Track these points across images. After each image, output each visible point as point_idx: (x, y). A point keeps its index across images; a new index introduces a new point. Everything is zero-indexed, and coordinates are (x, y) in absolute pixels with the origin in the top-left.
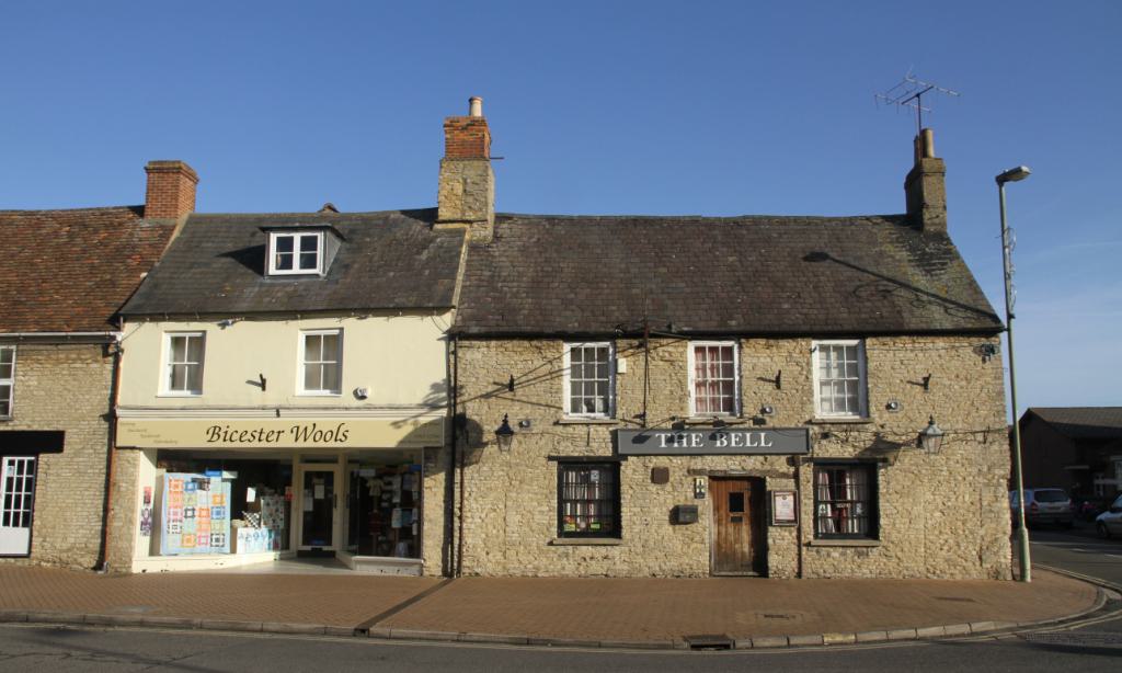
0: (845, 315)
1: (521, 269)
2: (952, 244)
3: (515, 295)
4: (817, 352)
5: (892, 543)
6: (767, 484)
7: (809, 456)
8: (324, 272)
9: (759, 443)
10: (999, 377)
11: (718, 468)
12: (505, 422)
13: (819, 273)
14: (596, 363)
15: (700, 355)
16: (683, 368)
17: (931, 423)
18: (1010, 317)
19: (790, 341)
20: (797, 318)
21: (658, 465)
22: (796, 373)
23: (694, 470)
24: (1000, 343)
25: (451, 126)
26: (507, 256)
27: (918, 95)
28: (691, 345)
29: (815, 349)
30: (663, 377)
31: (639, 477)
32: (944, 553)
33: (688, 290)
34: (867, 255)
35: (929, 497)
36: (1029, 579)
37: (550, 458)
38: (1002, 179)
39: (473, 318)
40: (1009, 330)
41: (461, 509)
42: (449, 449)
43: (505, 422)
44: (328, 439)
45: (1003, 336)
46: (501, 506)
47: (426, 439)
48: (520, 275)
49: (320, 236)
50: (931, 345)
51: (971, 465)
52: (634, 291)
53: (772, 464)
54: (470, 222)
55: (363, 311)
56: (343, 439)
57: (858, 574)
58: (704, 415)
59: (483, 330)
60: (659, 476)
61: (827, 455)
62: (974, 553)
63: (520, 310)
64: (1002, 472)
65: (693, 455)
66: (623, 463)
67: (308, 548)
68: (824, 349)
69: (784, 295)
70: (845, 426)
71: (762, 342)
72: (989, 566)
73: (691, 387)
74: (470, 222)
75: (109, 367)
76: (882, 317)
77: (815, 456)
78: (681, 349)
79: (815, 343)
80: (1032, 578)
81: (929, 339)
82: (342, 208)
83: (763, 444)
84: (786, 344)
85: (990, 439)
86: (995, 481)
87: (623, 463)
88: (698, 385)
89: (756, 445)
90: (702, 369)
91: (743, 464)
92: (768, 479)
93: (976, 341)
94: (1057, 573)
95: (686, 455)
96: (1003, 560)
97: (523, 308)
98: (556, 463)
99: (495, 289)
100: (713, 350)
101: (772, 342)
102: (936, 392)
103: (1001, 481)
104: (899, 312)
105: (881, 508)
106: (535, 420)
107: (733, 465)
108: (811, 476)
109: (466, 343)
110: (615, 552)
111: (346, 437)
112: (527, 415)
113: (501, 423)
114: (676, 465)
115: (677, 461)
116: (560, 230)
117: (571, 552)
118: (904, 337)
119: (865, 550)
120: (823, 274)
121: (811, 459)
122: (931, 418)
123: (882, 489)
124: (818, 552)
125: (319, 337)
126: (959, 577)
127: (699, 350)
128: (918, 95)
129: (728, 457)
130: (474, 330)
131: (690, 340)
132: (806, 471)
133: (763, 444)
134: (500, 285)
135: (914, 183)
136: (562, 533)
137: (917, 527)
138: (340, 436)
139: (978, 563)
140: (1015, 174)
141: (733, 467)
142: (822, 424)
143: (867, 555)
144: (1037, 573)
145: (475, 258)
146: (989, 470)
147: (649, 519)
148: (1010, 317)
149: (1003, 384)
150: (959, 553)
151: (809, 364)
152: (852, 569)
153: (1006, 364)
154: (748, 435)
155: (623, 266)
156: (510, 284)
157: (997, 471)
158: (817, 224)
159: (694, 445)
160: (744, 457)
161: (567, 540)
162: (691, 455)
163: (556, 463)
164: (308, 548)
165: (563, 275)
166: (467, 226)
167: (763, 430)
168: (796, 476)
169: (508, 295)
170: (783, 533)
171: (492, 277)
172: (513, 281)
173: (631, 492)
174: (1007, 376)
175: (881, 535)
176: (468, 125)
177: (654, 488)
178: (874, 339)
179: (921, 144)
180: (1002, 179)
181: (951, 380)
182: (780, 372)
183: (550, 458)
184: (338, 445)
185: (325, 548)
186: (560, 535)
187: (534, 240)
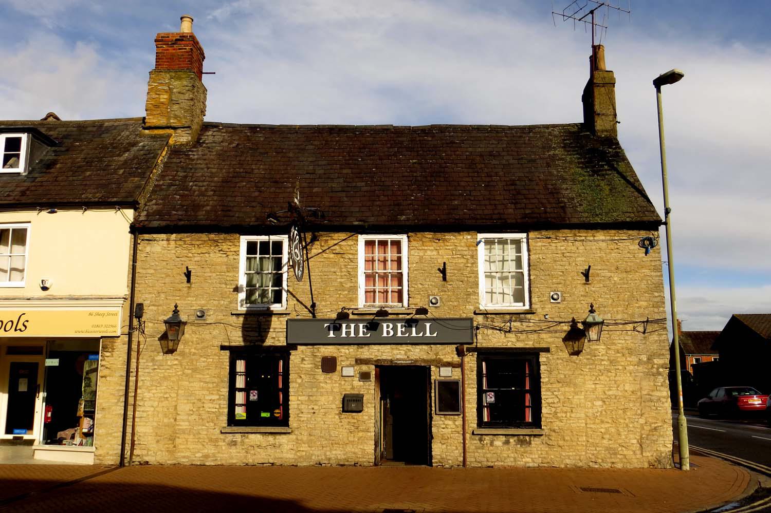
0: (511, 211)
1: (214, 170)
2: (620, 148)
3: (202, 194)
4: (482, 245)
5: (554, 431)
6: (432, 373)
7: (474, 346)
8: (25, 172)
9: (425, 333)
10: (658, 269)
11: (384, 357)
12: (176, 312)
13: (493, 174)
14: (258, 256)
15: (370, 248)
16: (354, 260)
17: (592, 311)
18: (667, 212)
19: (456, 234)
20: (465, 214)
21: (326, 355)
22: (462, 265)
23: (361, 360)
24: (658, 237)
25: (161, 40)
26: (205, 160)
27: (592, 12)
28: (362, 238)
29: (480, 242)
30: (601, 353)
31: (307, 365)
32: (605, 441)
33: (365, 189)
34: (541, 158)
35: (590, 385)
36: (687, 467)
37: (223, 348)
38: (659, 83)
39: (158, 213)
40: (666, 224)
41: (135, 397)
42: (126, 339)
43: (176, 312)
44: (8, 328)
45: (662, 228)
46: (174, 395)
47: (102, 329)
48: (212, 175)
49: (24, 137)
50: (592, 238)
51: (631, 354)
52: (315, 190)
53: (437, 354)
54: (175, 128)
55: (52, 205)
56: (23, 328)
57: (521, 463)
58: (373, 306)
59: (163, 223)
60: (329, 365)
61: (490, 345)
62: (635, 441)
63: (204, 206)
64: (661, 362)
65: (361, 344)
66: (293, 352)
67: (10, 437)
68: (489, 242)
69: (457, 193)
70: (508, 317)
71: (429, 235)
72: (649, 454)
73: (361, 279)
74: (175, 128)
75: (438, 370)
76: (546, 212)
77: (479, 346)
78: (350, 243)
79: (481, 236)
80: (691, 465)
81: (590, 233)
82: (65, 117)
83: (428, 334)
84: (452, 237)
85: (649, 328)
86: (654, 370)
87: (293, 352)
88: (369, 277)
89: (407, 335)
90: (370, 261)
91: (409, 353)
92: (433, 368)
93: (643, 234)
94: (726, 459)
95: (354, 344)
96: (662, 449)
97: (208, 205)
98: (227, 353)
99: (185, 188)
100: (383, 244)
101: (439, 235)
102: (595, 286)
103: (661, 370)
104: (563, 208)
105: (543, 397)
106: (208, 310)
107: (400, 355)
108: (474, 365)
109: (147, 236)
110: (283, 439)
111: (26, 327)
112: (202, 306)
113: (170, 315)
114: (344, 354)
115: (345, 350)
116: (261, 137)
117: (239, 440)
118: (566, 231)
119: (527, 438)
120: (497, 174)
121: (476, 349)
122: (592, 306)
123: (544, 379)
124: (481, 440)
125: (8, 230)
126: (619, 466)
127: (369, 244)
128: (592, 12)
129: (394, 346)
130: (155, 224)
131: (362, 233)
132: (471, 361)
133: (428, 334)
134: (191, 184)
135: (588, 97)
136: (232, 420)
137: (578, 415)
138: (20, 326)
139: (638, 452)
140: (672, 77)
141: (398, 357)
142: (486, 314)
143: (530, 443)
144: (698, 459)
145: (174, 160)
146: (648, 359)
147: (316, 407)
148: (667, 212)
149: (662, 276)
150: (620, 441)
151: (474, 257)
152: (515, 458)
153: (664, 258)
154: (428, 325)
155: (311, 168)
156: (200, 184)
157: (655, 361)
158: (497, 132)
159: (361, 335)
160: (410, 347)
161: (235, 429)
162: (358, 344)
163: (227, 353)
164: (10, 437)
165: (252, 176)
166: (171, 131)
167: (428, 320)
168: (461, 365)
169: (196, 193)
170: (447, 422)
171: (186, 177)
172: (204, 181)
173: (299, 381)
174: (665, 267)
175: (543, 423)
176: (177, 40)
177: (321, 376)
178: (536, 233)
179: (595, 61)
180: (659, 83)
181: (610, 271)
182: (444, 263)
183: (223, 348)
184: (18, 334)
185: (26, 437)
186: (229, 425)
187: (234, 145)
